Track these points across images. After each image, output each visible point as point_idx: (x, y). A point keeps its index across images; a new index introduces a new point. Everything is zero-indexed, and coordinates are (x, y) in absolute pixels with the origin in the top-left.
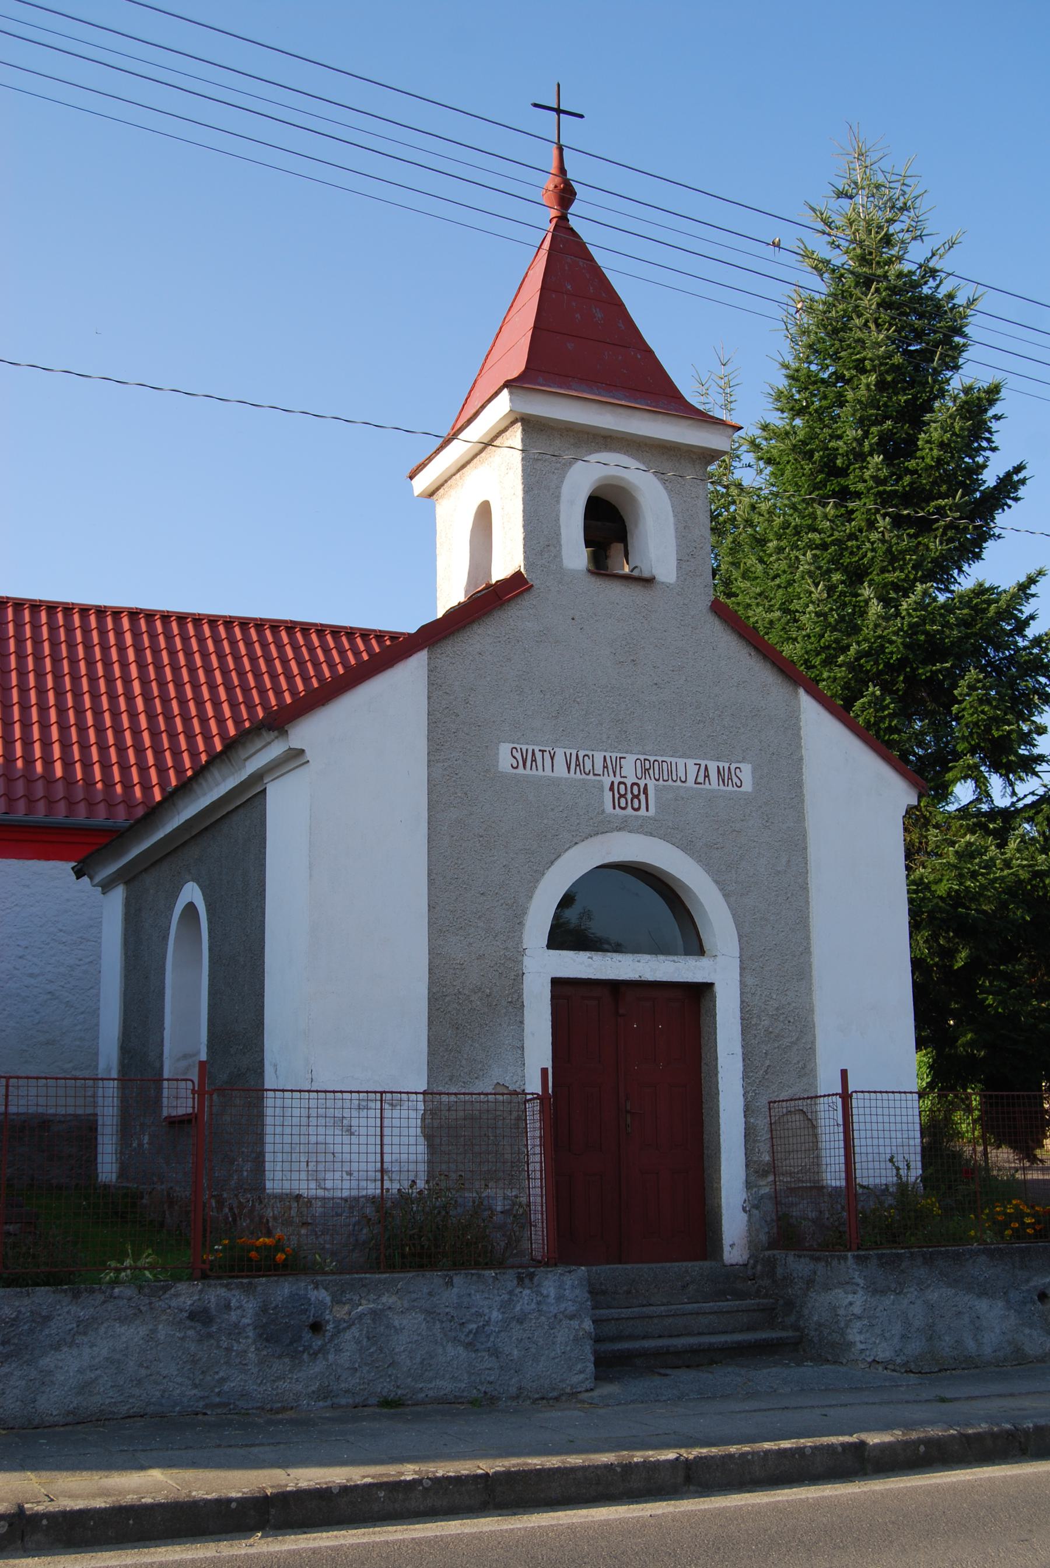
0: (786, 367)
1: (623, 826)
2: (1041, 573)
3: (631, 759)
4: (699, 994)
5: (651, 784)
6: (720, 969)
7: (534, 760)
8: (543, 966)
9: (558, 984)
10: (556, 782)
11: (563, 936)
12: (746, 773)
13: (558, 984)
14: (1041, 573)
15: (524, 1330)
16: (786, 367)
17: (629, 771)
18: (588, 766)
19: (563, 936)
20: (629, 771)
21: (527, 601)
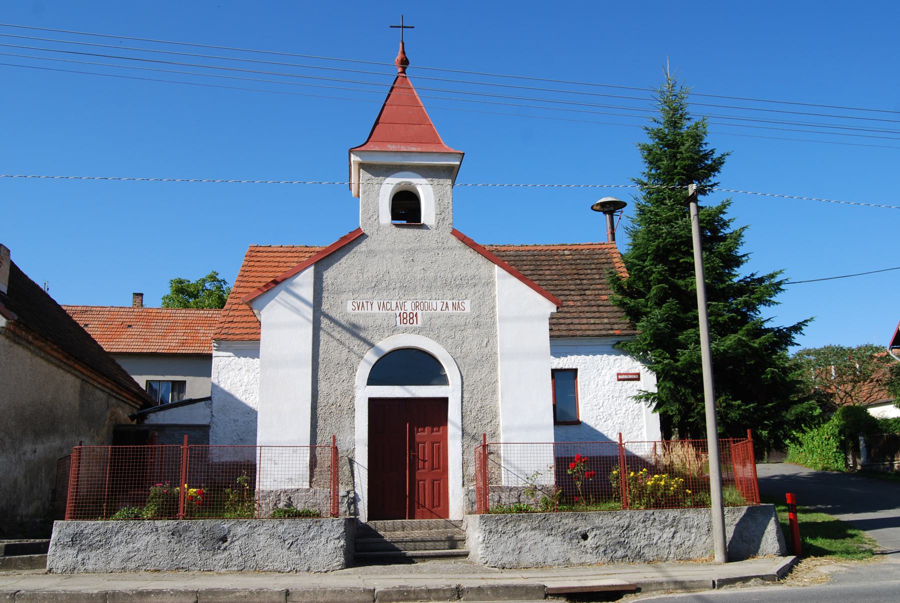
0: (627, 229)
1: (405, 331)
2: (811, 319)
3: (409, 302)
4: (445, 401)
5: (419, 313)
6: (451, 391)
7: (363, 306)
8: (365, 393)
9: (373, 403)
10: (373, 315)
11: (373, 380)
12: (467, 304)
13: (373, 403)
14: (811, 319)
15: (812, 452)
16: (627, 229)
17: (409, 307)
18: (389, 307)
19: (373, 380)
20: (409, 307)
21: (362, 247)
